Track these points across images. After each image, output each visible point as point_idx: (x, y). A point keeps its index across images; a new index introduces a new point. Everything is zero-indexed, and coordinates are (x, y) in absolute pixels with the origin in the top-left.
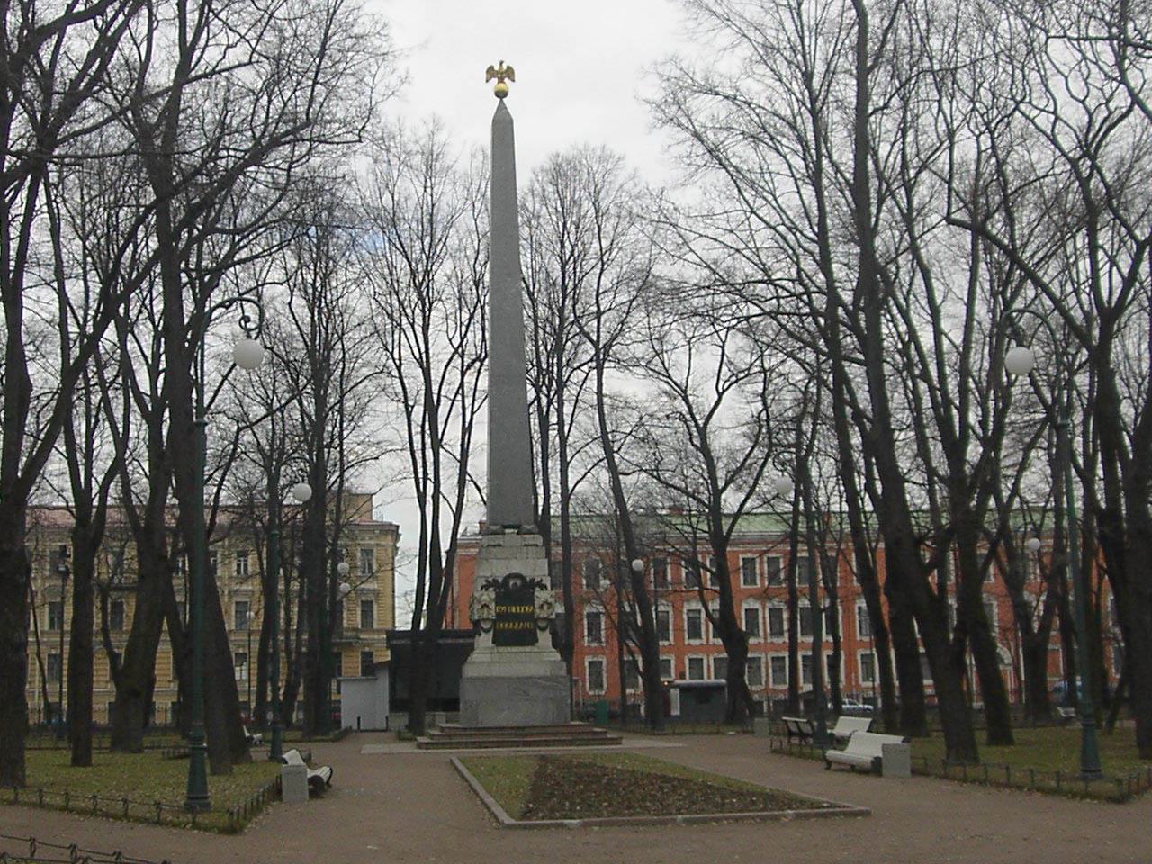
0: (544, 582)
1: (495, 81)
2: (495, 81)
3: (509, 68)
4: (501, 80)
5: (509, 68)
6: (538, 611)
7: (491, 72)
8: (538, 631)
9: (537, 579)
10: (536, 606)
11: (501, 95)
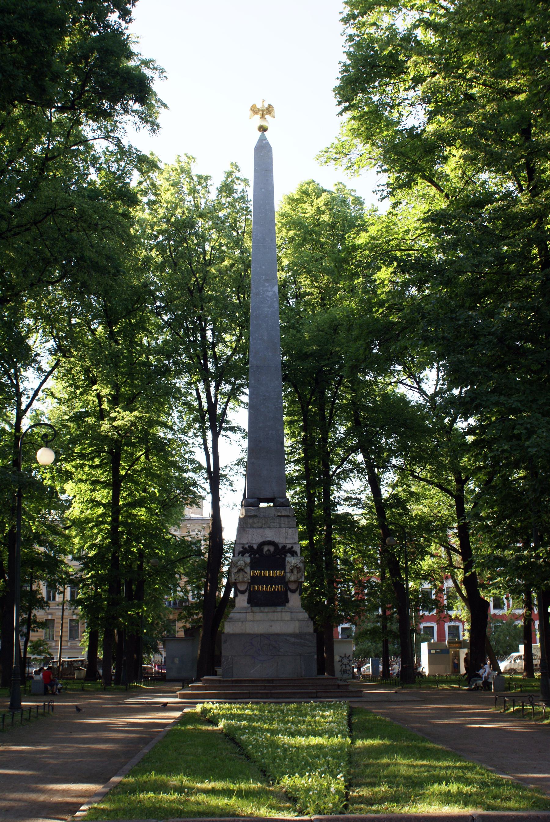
0: (294, 549)
1: (258, 116)
2: (258, 116)
3: (270, 106)
4: (263, 117)
5: (270, 106)
6: (288, 575)
7: (254, 110)
9: (289, 546)
10: (288, 570)
11: (263, 129)
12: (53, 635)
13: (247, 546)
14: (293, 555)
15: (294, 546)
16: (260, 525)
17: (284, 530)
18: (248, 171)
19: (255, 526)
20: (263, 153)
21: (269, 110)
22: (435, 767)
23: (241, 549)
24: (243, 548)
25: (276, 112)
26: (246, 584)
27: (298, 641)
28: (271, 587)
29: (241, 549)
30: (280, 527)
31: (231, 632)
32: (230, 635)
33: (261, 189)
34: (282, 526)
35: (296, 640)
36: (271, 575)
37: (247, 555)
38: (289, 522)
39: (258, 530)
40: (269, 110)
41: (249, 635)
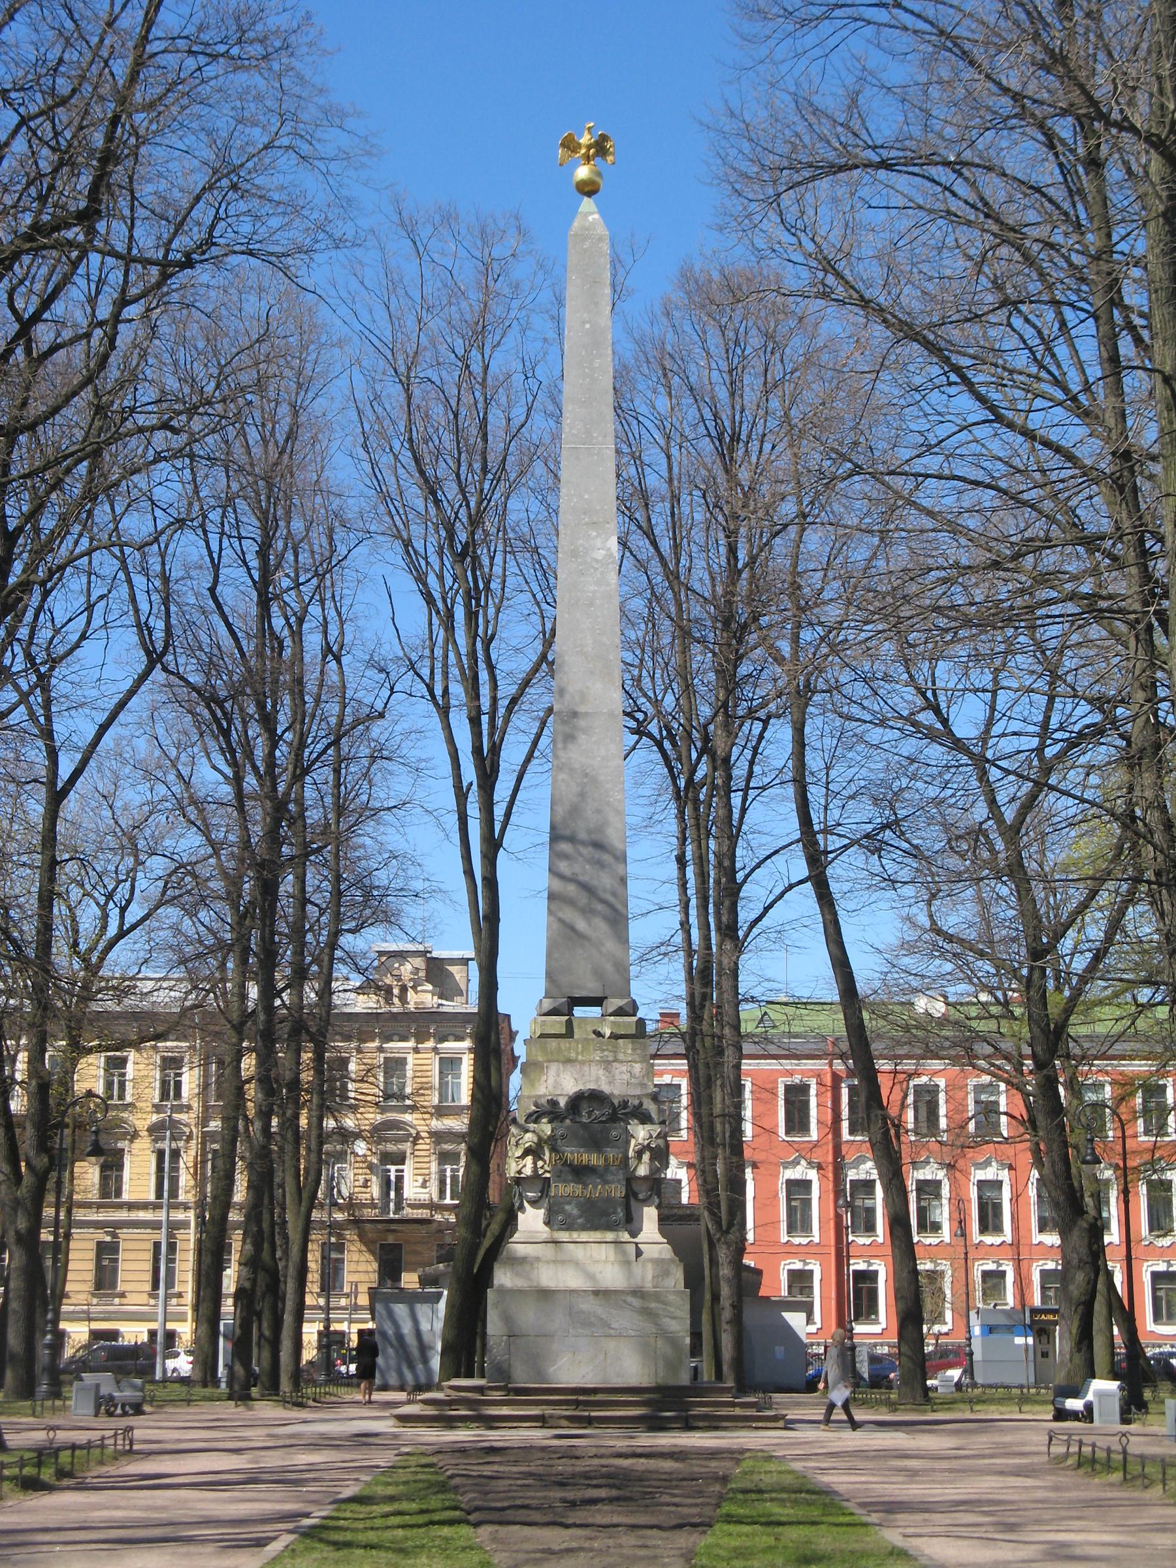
14: (643, 1123)
24: (536, 1105)
28: (595, 1187)
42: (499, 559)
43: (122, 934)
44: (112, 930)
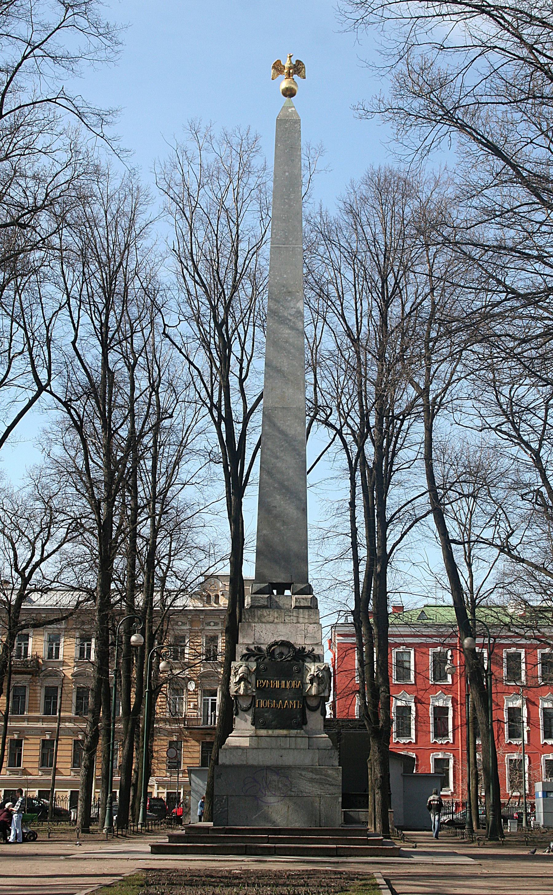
3: (298, 62)
5: (298, 62)
8: (307, 712)
12: (20, 755)
13: (252, 647)
15: (316, 648)
16: (271, 619)
17: (302, 626)
18: (266, 156)
19: (264, 620)
20: (288, 130)
21: (298, 68)
22: (413, 847)
23: (245, 652)
24: (248, 649)
25: (308, 70)
26: (251, 698)
27: (318, 777)
29: (245, 652)
30: (298, 622)
31: (227, 763)
32: (224, 766)
33: (285, 172)
34: (301, 620)
35: (314, 776)
36: (277, 682)
37: (253, 659)
38: (309, 615)
39: (268, 626)
40: (298, 68)
41: (252, 767)
42: (251, 329)
43: (42, 560)
44: (37, 558)
